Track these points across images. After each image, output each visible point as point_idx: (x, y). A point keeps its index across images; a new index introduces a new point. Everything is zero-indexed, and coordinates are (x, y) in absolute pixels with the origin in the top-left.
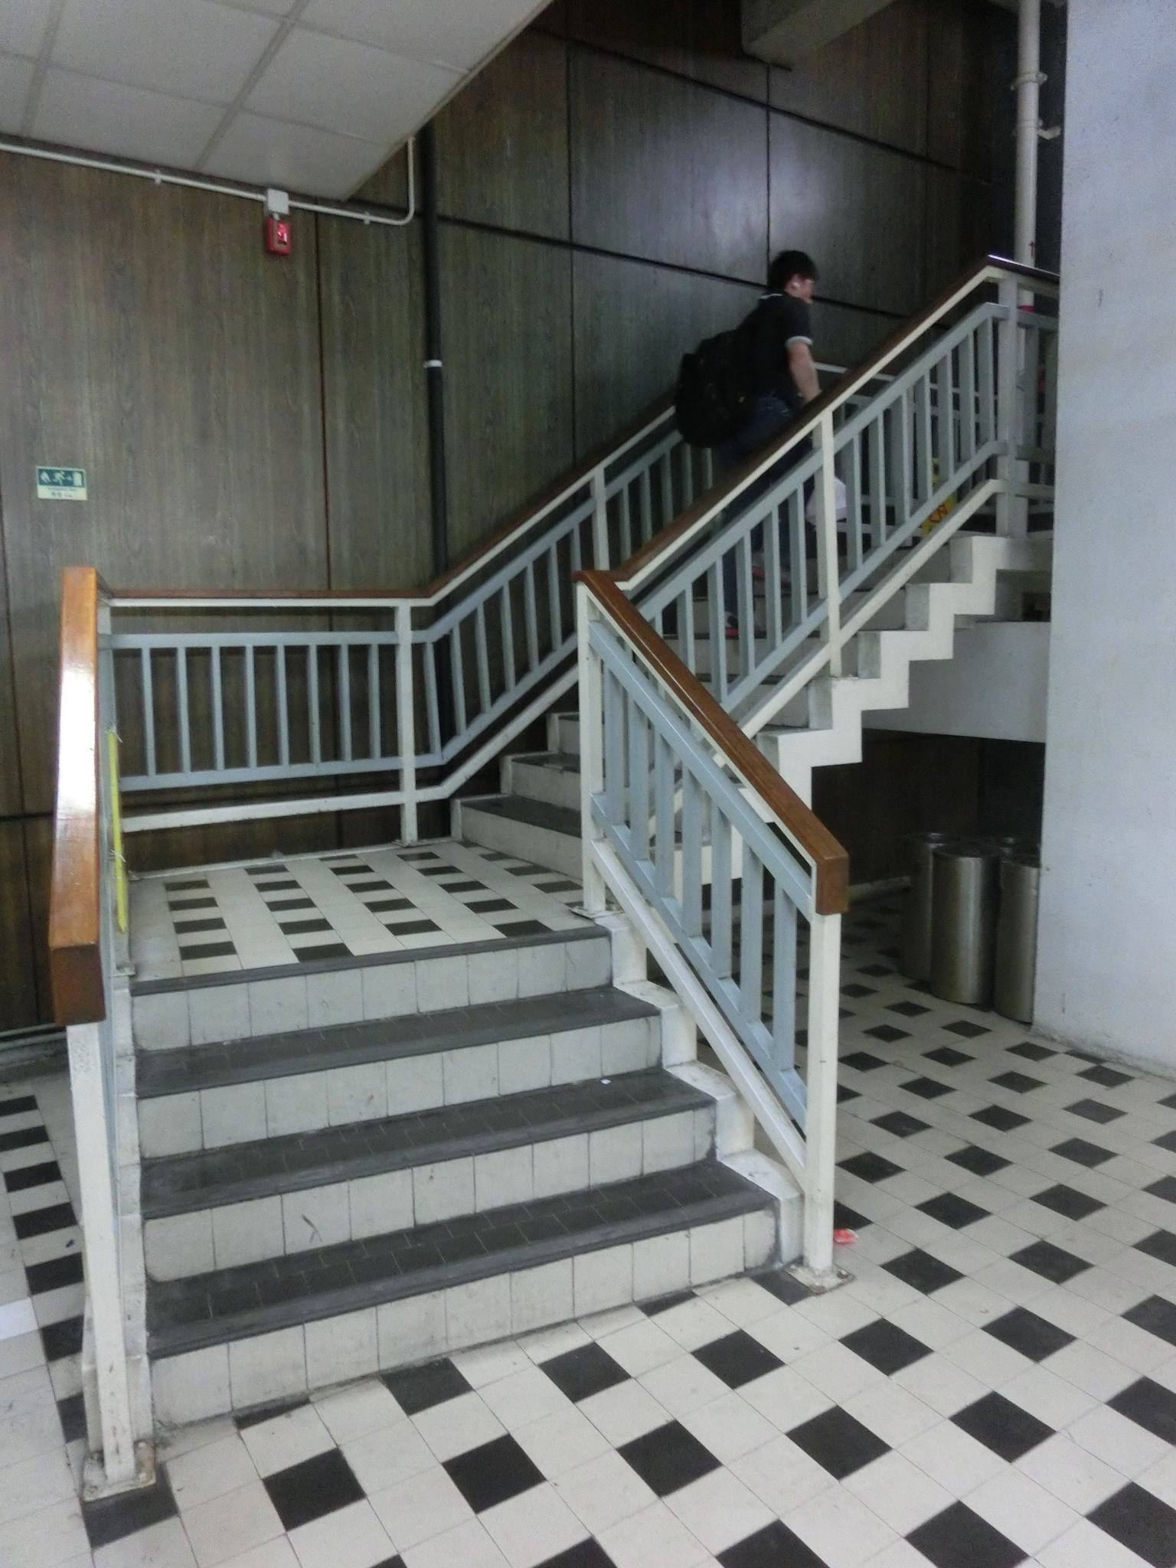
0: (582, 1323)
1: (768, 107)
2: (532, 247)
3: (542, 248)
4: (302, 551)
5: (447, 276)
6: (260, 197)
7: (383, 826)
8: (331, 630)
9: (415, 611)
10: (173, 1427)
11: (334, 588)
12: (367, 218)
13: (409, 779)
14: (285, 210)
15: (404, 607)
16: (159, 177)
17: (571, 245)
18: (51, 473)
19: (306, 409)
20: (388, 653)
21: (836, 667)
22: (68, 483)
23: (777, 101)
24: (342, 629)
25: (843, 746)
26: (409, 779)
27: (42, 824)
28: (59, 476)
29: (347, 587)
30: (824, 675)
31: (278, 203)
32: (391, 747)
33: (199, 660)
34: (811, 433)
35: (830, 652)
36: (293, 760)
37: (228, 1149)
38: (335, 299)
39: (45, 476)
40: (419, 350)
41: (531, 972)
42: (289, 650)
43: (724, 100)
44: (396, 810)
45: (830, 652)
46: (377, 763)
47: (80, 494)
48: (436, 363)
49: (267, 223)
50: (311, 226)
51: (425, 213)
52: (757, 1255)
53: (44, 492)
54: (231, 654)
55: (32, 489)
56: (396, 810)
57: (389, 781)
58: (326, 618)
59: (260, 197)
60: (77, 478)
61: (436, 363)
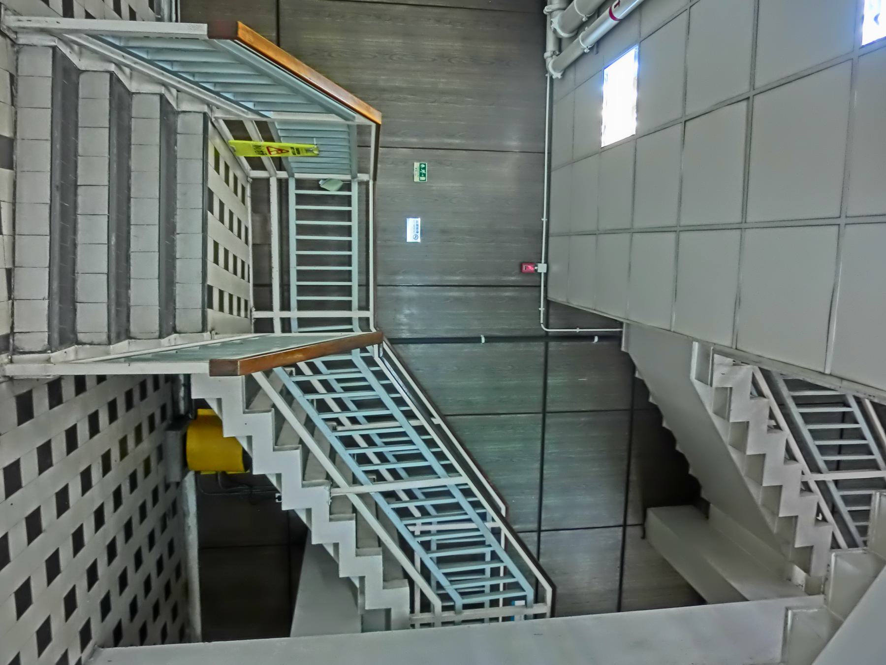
0: (11, 238)
1: (624, 526)
2: (541, 391)
3: (540, 396)
4: (395, 273)
5: (522, 347)
6: (543, 261)
7: (263, 303)
8: (359, 285)
9: (368, 319)
10: (18, 52)
11: (379, 288)
12: (542, 309)
13: (285, 314)
14: (539, 265)
15: (369, 314)
16: (544, 220)
17: (544, 412)
18: (424, 168)
19: (458, 278)
20: (347, 306)
21: (336, 492)
22: (421, 175)
23: (629, 529)
24: (359, 291)
25: (293, 499)
26: (285, 314)
27: (266, 248)
28: (423, 171)
29: (379, 294)
30: (334, 485)
31: (542, 268)
32: (302, 306)
33: (347, 277)
34: (457, 472)
35: (345, 489)
36: (298, 256)
37: (129, 128)
38: (508, 293)
39: (423, 166)
40: (489, 333)
41: (189, 295)
42: (350, 272)
43: (623, 499)
44: (271, 309)
45: (345, 489)
46: (294, 298)
47: (417, 179)
48: (483, 340)
49: (535, 264)
50: (533, 284)
51: (547, 338)
52: (20, 341)
53: (417, 165)
54: (348, 246)
55: (418, 161)
56: (271, 309)
57: (285, 305)
58: (364, 282)
59: (543, 261)
60: (423, 178)
61: (483, 340)
